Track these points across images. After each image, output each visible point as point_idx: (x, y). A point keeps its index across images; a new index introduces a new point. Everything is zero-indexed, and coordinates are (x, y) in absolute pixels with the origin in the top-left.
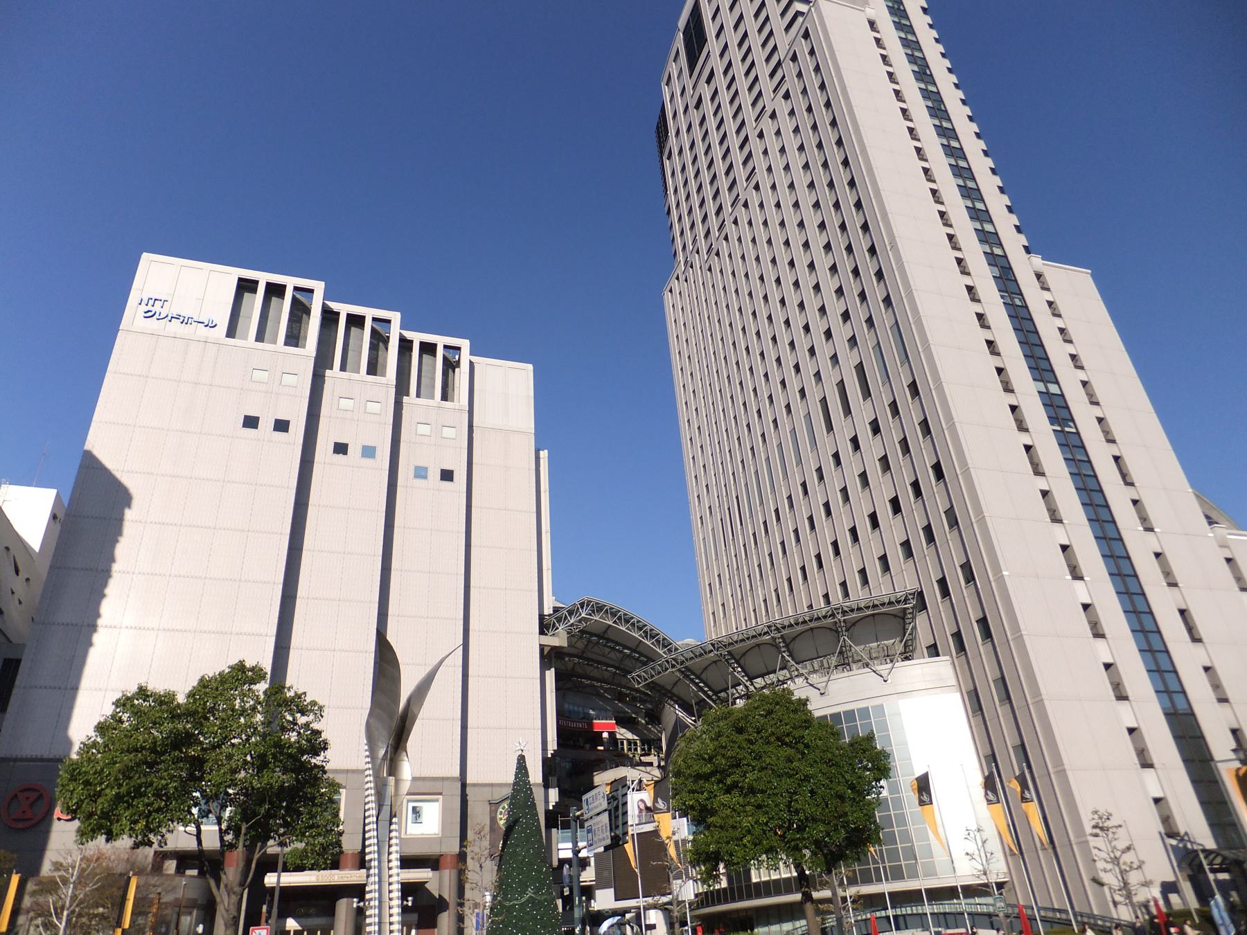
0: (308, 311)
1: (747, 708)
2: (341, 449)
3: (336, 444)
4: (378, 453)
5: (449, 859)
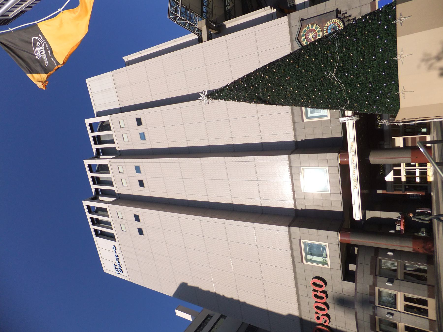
0: (100, 165)
1: (348, 109)
2: (139, 122)
3: (138, 125)
4: (138, 117)
5: (341, 160)
